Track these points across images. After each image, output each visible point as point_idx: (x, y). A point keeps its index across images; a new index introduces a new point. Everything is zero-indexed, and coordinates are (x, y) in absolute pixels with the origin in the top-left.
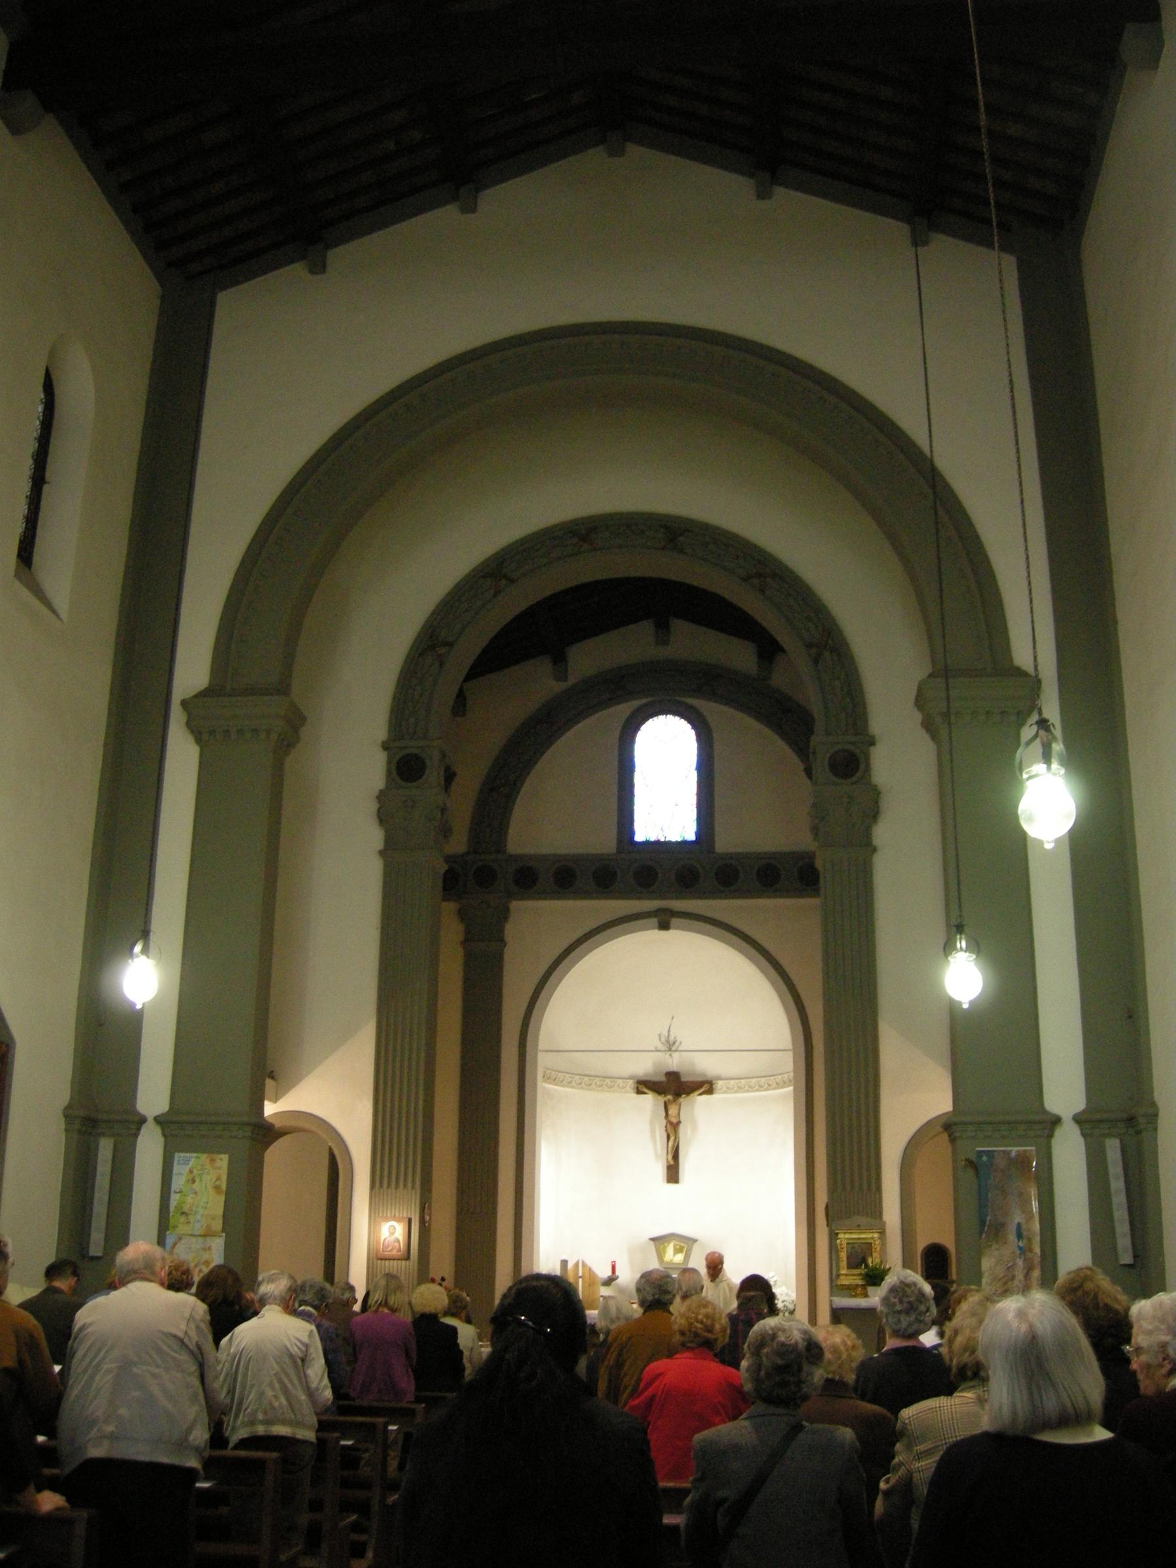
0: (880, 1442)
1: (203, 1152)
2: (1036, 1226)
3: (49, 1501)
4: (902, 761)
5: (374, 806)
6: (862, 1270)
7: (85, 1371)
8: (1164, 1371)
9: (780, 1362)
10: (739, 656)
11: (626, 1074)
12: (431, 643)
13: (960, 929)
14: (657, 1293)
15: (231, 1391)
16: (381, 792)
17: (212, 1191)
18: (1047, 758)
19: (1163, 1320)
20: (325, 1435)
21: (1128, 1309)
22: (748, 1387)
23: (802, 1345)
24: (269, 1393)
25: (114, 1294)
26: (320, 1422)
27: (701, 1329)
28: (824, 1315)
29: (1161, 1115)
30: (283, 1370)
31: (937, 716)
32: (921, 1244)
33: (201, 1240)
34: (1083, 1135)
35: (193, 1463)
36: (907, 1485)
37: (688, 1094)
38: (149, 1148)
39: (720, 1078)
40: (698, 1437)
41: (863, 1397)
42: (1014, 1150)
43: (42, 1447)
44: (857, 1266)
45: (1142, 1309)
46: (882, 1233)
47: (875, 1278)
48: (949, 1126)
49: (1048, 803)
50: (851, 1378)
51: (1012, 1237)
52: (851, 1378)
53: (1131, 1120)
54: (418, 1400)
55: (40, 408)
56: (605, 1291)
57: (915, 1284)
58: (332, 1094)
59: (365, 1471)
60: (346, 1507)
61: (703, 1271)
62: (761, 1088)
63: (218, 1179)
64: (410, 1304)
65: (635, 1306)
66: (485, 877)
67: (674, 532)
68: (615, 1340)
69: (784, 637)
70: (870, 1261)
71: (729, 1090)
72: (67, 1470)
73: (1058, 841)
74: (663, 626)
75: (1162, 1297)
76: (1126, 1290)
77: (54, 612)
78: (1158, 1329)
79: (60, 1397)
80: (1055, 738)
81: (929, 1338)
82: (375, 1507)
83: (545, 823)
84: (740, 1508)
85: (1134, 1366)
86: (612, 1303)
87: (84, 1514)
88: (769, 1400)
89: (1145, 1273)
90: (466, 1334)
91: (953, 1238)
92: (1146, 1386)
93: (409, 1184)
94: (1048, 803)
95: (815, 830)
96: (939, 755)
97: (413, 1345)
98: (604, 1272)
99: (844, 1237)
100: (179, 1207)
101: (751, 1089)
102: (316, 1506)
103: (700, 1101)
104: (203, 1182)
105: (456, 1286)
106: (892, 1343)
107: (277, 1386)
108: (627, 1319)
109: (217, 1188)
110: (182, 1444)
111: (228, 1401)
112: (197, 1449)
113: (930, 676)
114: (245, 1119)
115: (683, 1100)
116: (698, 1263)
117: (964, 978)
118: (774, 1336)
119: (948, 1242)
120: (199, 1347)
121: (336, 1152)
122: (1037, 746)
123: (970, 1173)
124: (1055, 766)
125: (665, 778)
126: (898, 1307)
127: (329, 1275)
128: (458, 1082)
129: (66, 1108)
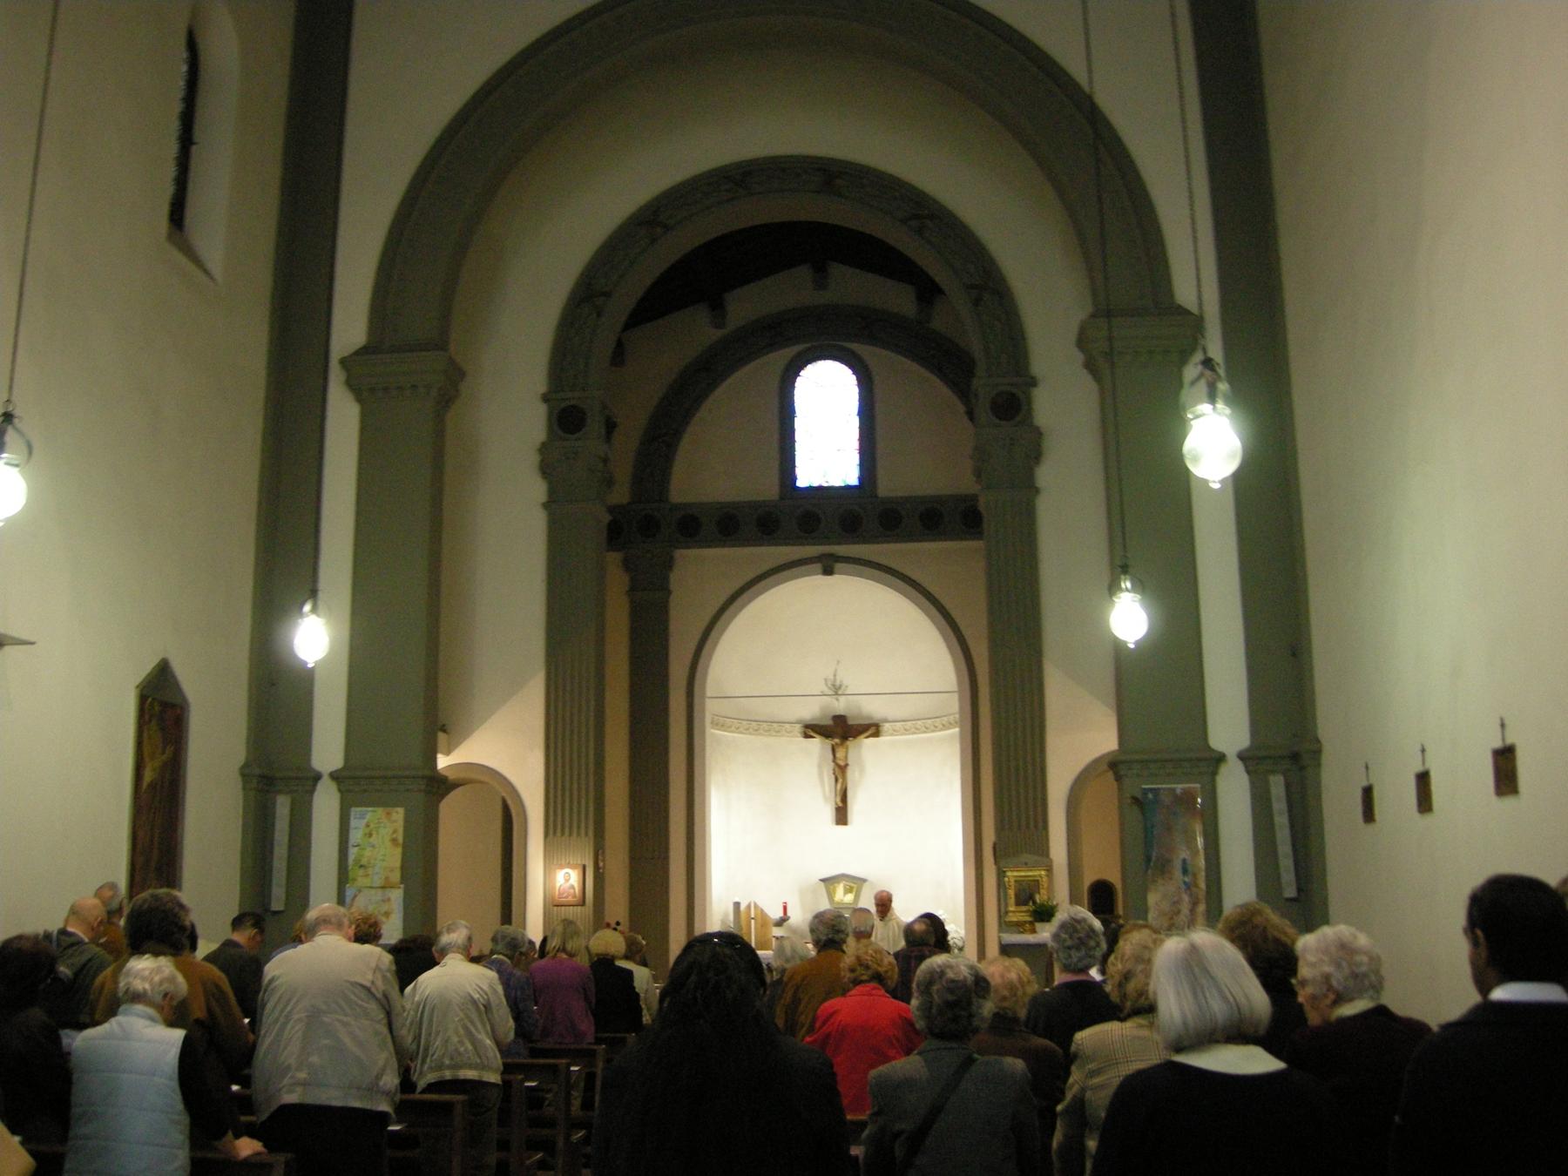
0: (1052, 1069)
1: (378, 805)
2: (1202, 862)
3: (247, 1147)
4: (1064, 402)
5: (535, 459)
6: (1031, 907)
7: (277, 1020)
8: (1328, 1002)
9: (950, 998)
10: (899, 299)
11: (793, 719)
12: (587, 294)
13: (1125, 569)
14: (831, 932)
15: (417, 1038)
16: (543, 444)
17: (388, 844)
18: (1212, 398)
19: (1326, 951)
20: (508, 1077)
21: (1294, 942)
22: (920, 1024)
23: (970, 979)
24: (455, 1039)
25: (301, 948)
26: (506, 1065)
27: (869, 963)
28: (992, 949)
29: (1326, 758)
30: (468, 1017)
31: (1099, 355)
32: (1089, 879)
33: (380, 892)
34: (1248, 772)
35: (384, 1107)
36: (1080, 1104)
37: (855, 737)
38: (326, 803)
39: (886, 721)
40: (873, 1073)
41: (1035, 1032)
42: (1179, 787)
43: (235, 1095)
44: (1025, 903)
45: (1307, 944)
46: (1049, 870)
47: (1044, 914)
48: (1114, 765)
49: (1213, 443)
50: (1022, 1014)
51: (1178, 873)
52: (1022, 1014)
53: (1295, 757)
54: (598, 1041)
55: (184, 68)
56: (777, 932)
57: (1085, 920)
58: (503, 744)
59: (548, 1111)
60: (533, 1146)
61: (873, 909)
62: (927, 730)
63: (395, 831)
64: (587, 948)
65: (810, 946)
66: (649, 527)
67: (830, 175)
68: (791, 978)
69: (940, 274)
70: (1038, 898)
71: (895, 732)
72: (264, 1117)
73: (1222, 482)
74: (820, 270)
75: (1327, 931)
76: (1294, 922)
77: (206, 272)
78: (1322, 960)
79: (253, 1048)
80: (1219, 377)
81: (1094, 973)
82: (561, 1143)
83: (706, 472)
84: (917, 1139)
85: (1300, 999)
86: (787, 944)
87: (280, 1159)
88: (940, 1036)
89: (1309, 906)
90: (642, 976)
91: (1119, 876)
92: (1314, 1018)
93: (583, 831)
94: (1213, 443)
95: (978, 473)
96: (1102, 392)
97: (592, 987)
98: (776, 914)
99: (1012, 875)
100: (357, 861)
101: (917, 730)
102: (504, 1145)
103: (867, 744)
104: (381, 835)
105: (631, 930)
106: (1060, 977)
107: (462, 1032)
108: (802, 958)
109: (394, 841)
110: (373, 1089)
111: (414, 1047)
112: (387, 1093)
113: (1093, 316)
114: (420, 773)
115: (851, 743)
116: (868, 902)
117: (1129, 618)
118: (942, 973)
119: (1115, 878)
120: (386, 996)
121: (509, 802)
122: (1202, 386)
123: (1135, 808)
124: (1220, 405)
125: (827, 423)
126: (1069, 943)
127: (507, 918)
128: (627, 773)
129: (242, 768)
